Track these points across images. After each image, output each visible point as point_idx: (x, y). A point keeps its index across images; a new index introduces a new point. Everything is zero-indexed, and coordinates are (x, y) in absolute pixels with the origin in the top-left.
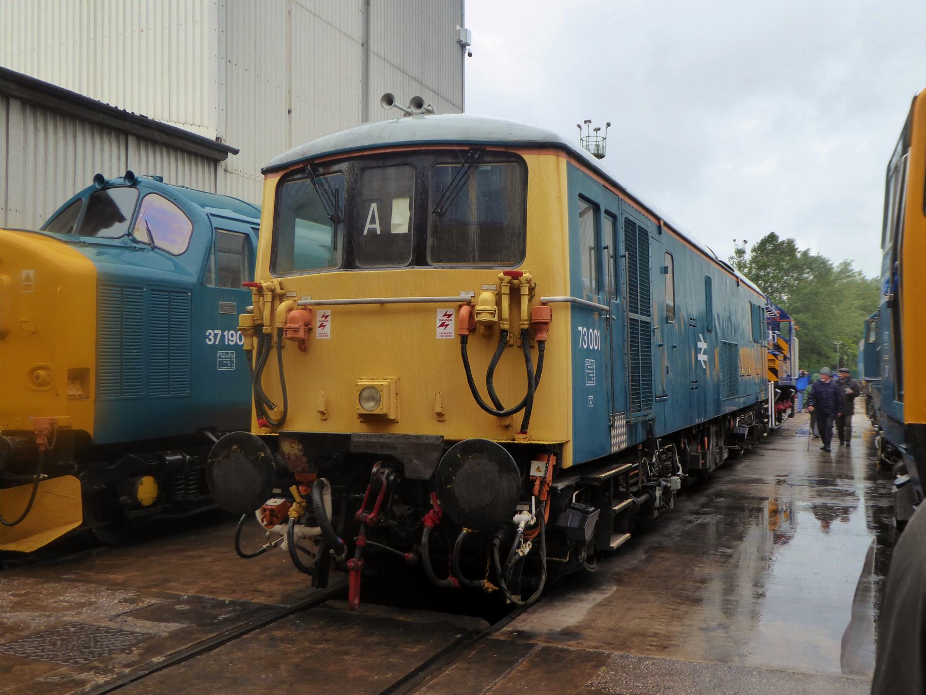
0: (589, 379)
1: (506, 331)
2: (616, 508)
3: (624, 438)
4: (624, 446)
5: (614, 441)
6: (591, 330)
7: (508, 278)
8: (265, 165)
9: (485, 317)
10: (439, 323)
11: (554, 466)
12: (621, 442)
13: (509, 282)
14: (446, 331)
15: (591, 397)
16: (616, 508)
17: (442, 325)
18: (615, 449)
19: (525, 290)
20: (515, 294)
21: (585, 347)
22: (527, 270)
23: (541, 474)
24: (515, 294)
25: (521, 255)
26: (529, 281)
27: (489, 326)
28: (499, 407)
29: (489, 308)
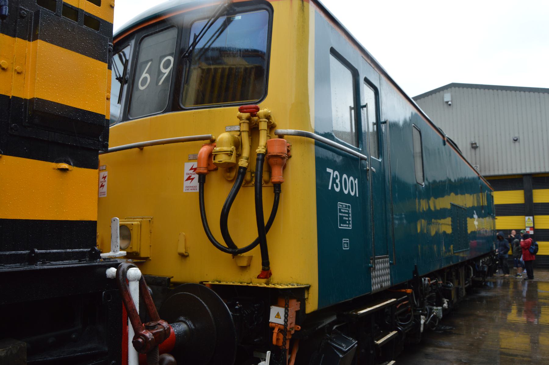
0: (344, 222)
1: (245, 169)
2: (379, 342)
3: (388, 277)
4: (387, 284)
5: (373, 281)
6: (345, 176)
7: (245, 115)
8: (253, 258)
9: (222, 158)
10: (186, 177)
11: (297, 312)
12: (384, 281)
13: (248, 119)
14: (192, 184)
15: (345, 240)
16: (379, 342)
17: (189, 179)
18: (375, 287)
19: (263, 126)
20: (254, 130)
21: (338, 190)
22: (264, 108)
23: (281, 321)
24: (254, 130)
25: (263, 94)
26: (268, 117)
27: (229, 167)
28: (235, 247)
29: (225, 148)
